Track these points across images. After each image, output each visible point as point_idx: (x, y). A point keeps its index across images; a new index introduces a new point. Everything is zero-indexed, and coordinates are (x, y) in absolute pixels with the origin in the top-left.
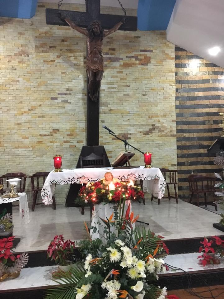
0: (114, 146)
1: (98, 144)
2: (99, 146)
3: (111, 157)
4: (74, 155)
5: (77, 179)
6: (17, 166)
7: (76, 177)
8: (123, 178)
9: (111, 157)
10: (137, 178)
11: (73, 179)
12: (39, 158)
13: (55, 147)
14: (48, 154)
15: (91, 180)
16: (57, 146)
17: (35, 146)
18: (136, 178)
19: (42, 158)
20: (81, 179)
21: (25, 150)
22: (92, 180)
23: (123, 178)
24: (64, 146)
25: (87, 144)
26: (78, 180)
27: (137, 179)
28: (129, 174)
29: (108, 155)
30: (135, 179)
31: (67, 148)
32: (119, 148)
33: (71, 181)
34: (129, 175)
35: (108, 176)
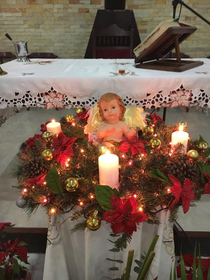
0: (152, 11)
1: (123, 7)
2: (125, 11)
3: (145, 31)
4: (86, 26)
5: (38, 96)
6: (4, 41)
7: (34, 92)
8: (159, 99)
9: (145, 31)
10: (195, 102)
11: (27, 96)
12: (33, 30)
13: (55, 11)
14: (45, 23)
15: (73, 100)
16: (59, 9)
17: (25, 9)
18: (193, 100)
19: (38, 30)
20: (48, 97)
21: (11, 16)
22: (75, 101)
23: (159, 99)
24: (70, 11)
25: (105, 8)
26: (40, 100)
27: (196, 104)
28: (175, 90)
29: (140, 27)
30: (191, 103)
31: (74, 14)
32: (159, 17)
33: (23, 101)
34: (174, 92)
35: (110, 109)
